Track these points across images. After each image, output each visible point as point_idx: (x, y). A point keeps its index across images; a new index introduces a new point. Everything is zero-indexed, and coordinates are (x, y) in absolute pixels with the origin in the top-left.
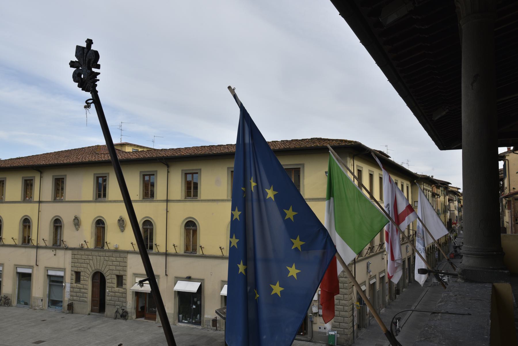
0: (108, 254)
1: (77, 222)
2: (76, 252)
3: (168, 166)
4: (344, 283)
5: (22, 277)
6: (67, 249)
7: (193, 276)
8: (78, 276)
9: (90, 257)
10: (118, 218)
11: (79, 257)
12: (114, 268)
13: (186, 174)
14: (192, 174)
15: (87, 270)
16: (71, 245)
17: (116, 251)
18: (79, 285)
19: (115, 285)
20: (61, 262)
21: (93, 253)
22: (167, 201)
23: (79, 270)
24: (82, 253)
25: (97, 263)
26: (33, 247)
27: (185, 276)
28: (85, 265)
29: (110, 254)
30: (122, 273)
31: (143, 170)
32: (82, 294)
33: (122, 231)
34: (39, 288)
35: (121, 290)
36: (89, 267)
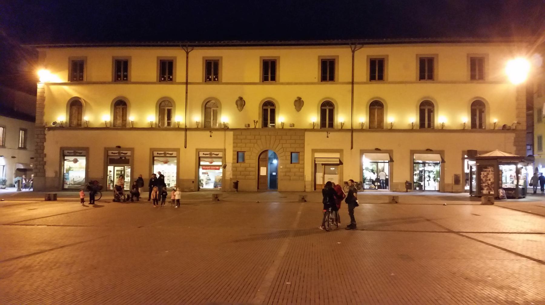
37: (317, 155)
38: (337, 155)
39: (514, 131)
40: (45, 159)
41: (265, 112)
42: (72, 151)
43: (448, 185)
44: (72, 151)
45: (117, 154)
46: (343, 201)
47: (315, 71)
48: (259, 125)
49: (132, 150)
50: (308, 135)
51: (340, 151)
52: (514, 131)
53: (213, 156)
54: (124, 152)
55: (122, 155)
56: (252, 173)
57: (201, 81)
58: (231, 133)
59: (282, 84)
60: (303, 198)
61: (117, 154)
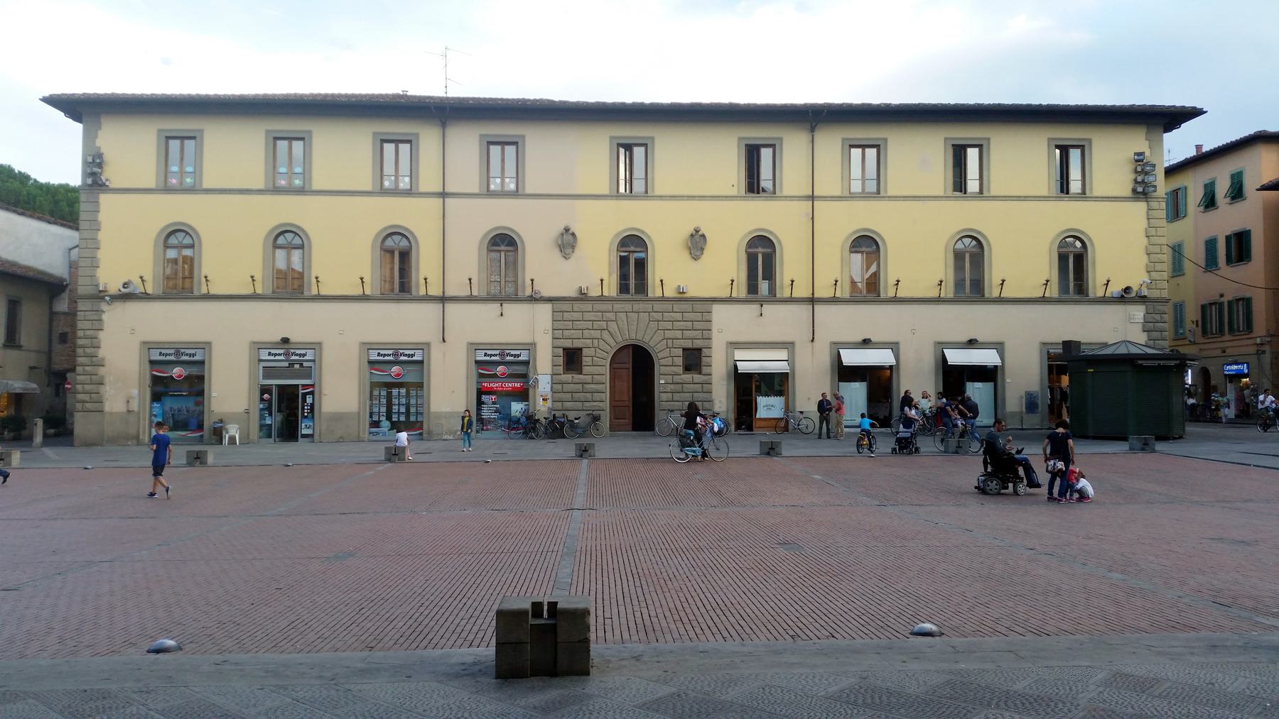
0: (658, 307)
1: (567, 242)
2: (560, 306)
3: (444, 125)
4: (83, 347)
5: (1050, 357)
6: (534, 299)
7: (980, 340)
8: (572, 359)
9: (611, 316)
10: (691, 230)
11: (577, 316)
12: (679, 334)
13: (276, 139)
14: (182, 138)
15: (602, 342)
16: (546, 293)
17: (681, 298)
18: (578, 377)
19: (680, 370)
20: (528, 329)
21: (617, 306)
22: (812, 198)
23: (577, 344)
24: (588, 306)
25: (632, 325)
26: (428, 299)
27: (965, 338)
28: (597, 334)
29: (668, 306)
30: (698, 344)
31: (484, 132)
32: (589, 395)
33: (696, 258)
34: (449, 393)
35: (697, 378)
36: (606, 335)
37: (739, 354)
38: (783, 354)
39: (1142, 299)
40: (102, 371)
41: (751, 260)
42: (390, 352)
43: (1013, 414)
44: (390, 352)
45: (282, 358)
46: (1070, 441)
47: (731, 172)
48: (611, 289)
49: (317, 346)
50: (719, 312)
51: (789, 346)
52: (1142, 299)
53: (403, 358)
54: (298, 352)
55: (294, 358)
56: (167, 408)
57: (734, 192)
58: (547, 308)
59: (661, 197)
60: (586, 451)
61: (282, 358)
